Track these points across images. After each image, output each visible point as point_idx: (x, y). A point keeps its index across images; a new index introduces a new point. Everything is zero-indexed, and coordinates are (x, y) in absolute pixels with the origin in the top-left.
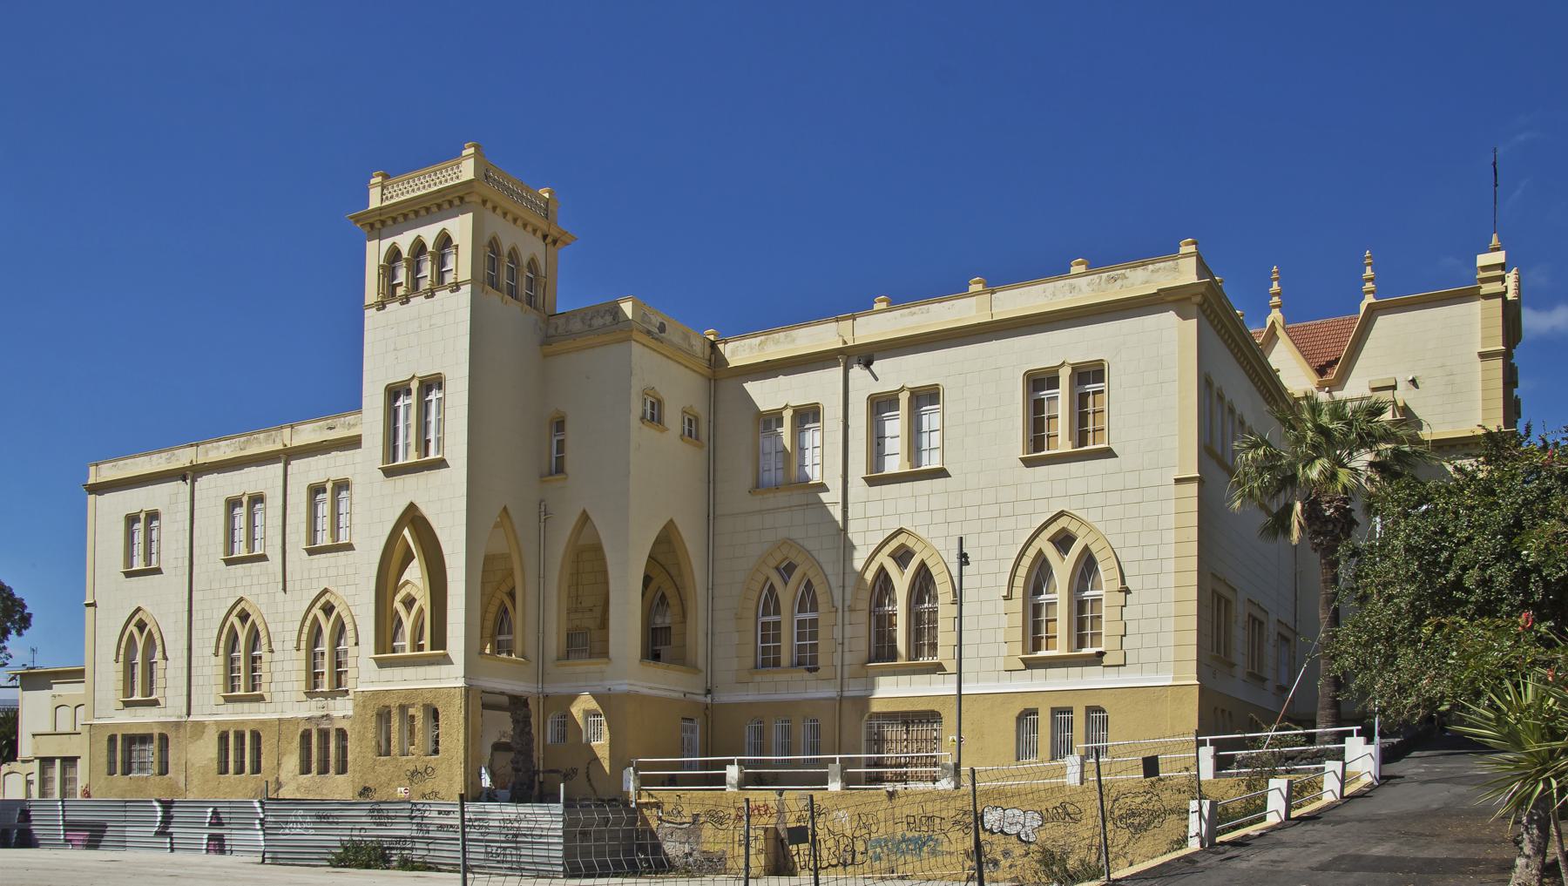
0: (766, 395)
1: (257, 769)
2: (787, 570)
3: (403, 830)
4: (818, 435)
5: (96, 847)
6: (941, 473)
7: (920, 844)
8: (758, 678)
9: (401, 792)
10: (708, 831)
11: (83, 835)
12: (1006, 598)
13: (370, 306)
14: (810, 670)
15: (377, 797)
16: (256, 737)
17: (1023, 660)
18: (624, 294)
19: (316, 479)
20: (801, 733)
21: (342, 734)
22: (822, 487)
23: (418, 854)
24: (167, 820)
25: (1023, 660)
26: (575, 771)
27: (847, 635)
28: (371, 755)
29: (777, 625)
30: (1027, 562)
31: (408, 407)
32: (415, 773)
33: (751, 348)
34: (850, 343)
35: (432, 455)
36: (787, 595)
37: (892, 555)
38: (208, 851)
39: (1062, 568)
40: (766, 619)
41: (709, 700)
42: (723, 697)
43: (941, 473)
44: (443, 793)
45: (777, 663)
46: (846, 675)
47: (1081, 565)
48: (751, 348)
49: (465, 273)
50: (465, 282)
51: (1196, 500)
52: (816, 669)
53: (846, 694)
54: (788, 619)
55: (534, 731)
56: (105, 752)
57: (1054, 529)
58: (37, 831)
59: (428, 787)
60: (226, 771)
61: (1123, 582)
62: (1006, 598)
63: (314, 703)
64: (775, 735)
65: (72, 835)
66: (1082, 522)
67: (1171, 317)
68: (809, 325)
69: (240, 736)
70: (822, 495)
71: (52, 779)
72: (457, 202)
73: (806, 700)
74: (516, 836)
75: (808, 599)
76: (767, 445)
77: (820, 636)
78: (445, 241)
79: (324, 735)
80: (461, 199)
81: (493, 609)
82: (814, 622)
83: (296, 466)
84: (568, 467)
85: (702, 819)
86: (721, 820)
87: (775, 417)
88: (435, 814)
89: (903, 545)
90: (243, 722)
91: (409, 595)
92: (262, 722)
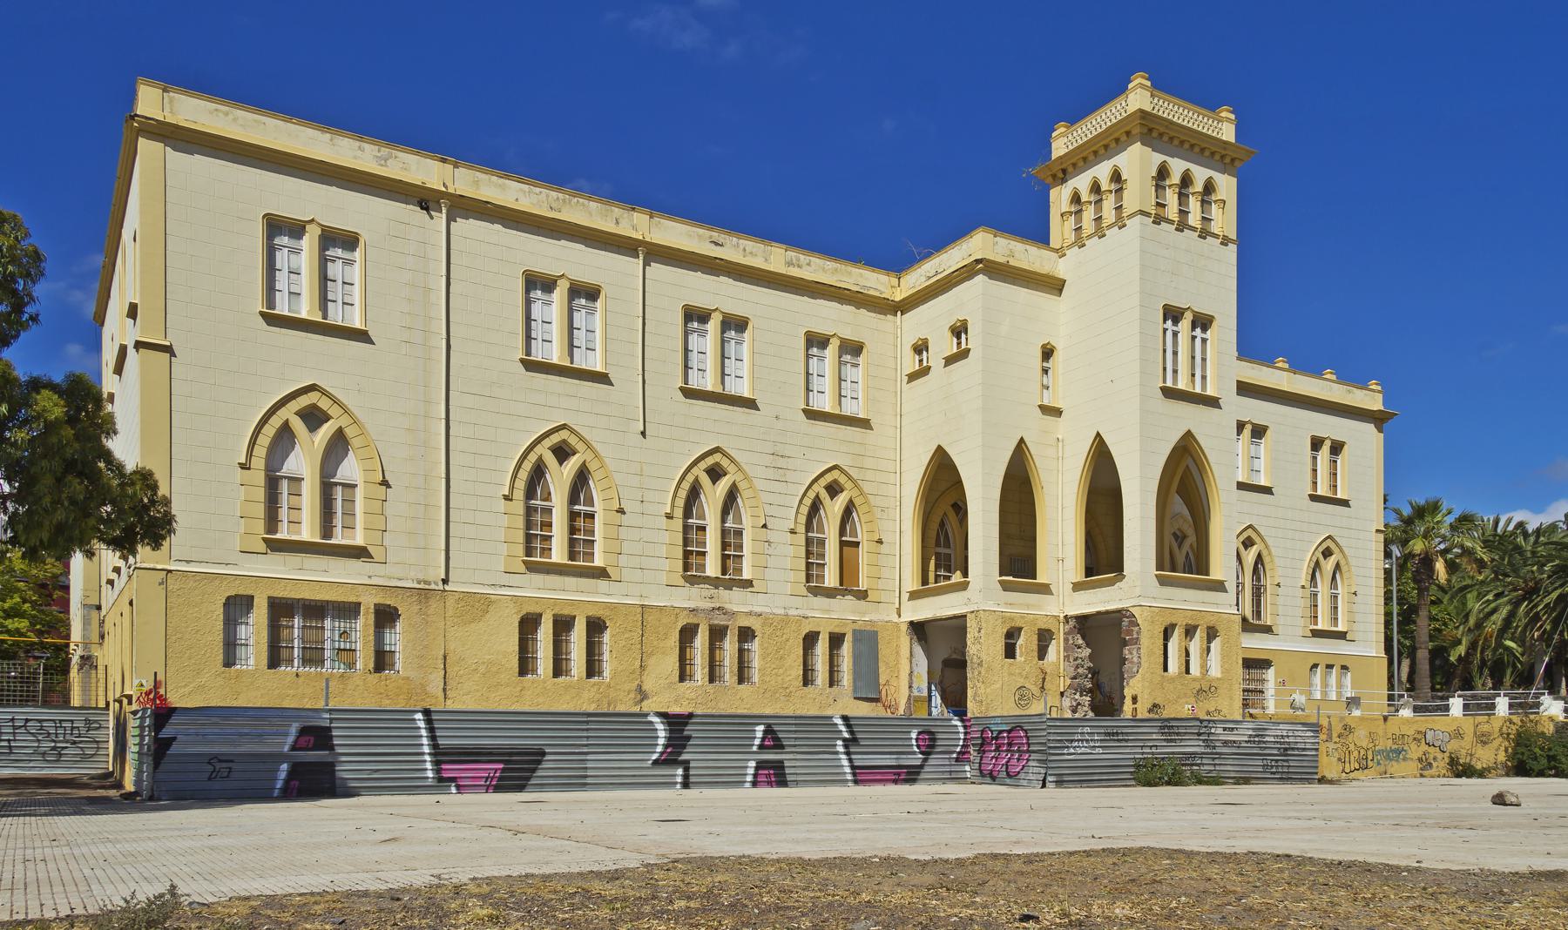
1: (593, 669)
3: (1193, 746)
5: (520, 788)
7: (1398, 752)
12: (244, 467)
15: (1165, 715)
17: (264, 540)
23: (1206, 769)
25: (264, 540)
38: (755, 784)
44: (1225, 711)
56: (220, 625)
58: (346, 770)
62: (244, 467)
63: (695, 590)
65: (450, 770)
67: (1370, 428)
88: (1220, 731)
91: (835, 481)
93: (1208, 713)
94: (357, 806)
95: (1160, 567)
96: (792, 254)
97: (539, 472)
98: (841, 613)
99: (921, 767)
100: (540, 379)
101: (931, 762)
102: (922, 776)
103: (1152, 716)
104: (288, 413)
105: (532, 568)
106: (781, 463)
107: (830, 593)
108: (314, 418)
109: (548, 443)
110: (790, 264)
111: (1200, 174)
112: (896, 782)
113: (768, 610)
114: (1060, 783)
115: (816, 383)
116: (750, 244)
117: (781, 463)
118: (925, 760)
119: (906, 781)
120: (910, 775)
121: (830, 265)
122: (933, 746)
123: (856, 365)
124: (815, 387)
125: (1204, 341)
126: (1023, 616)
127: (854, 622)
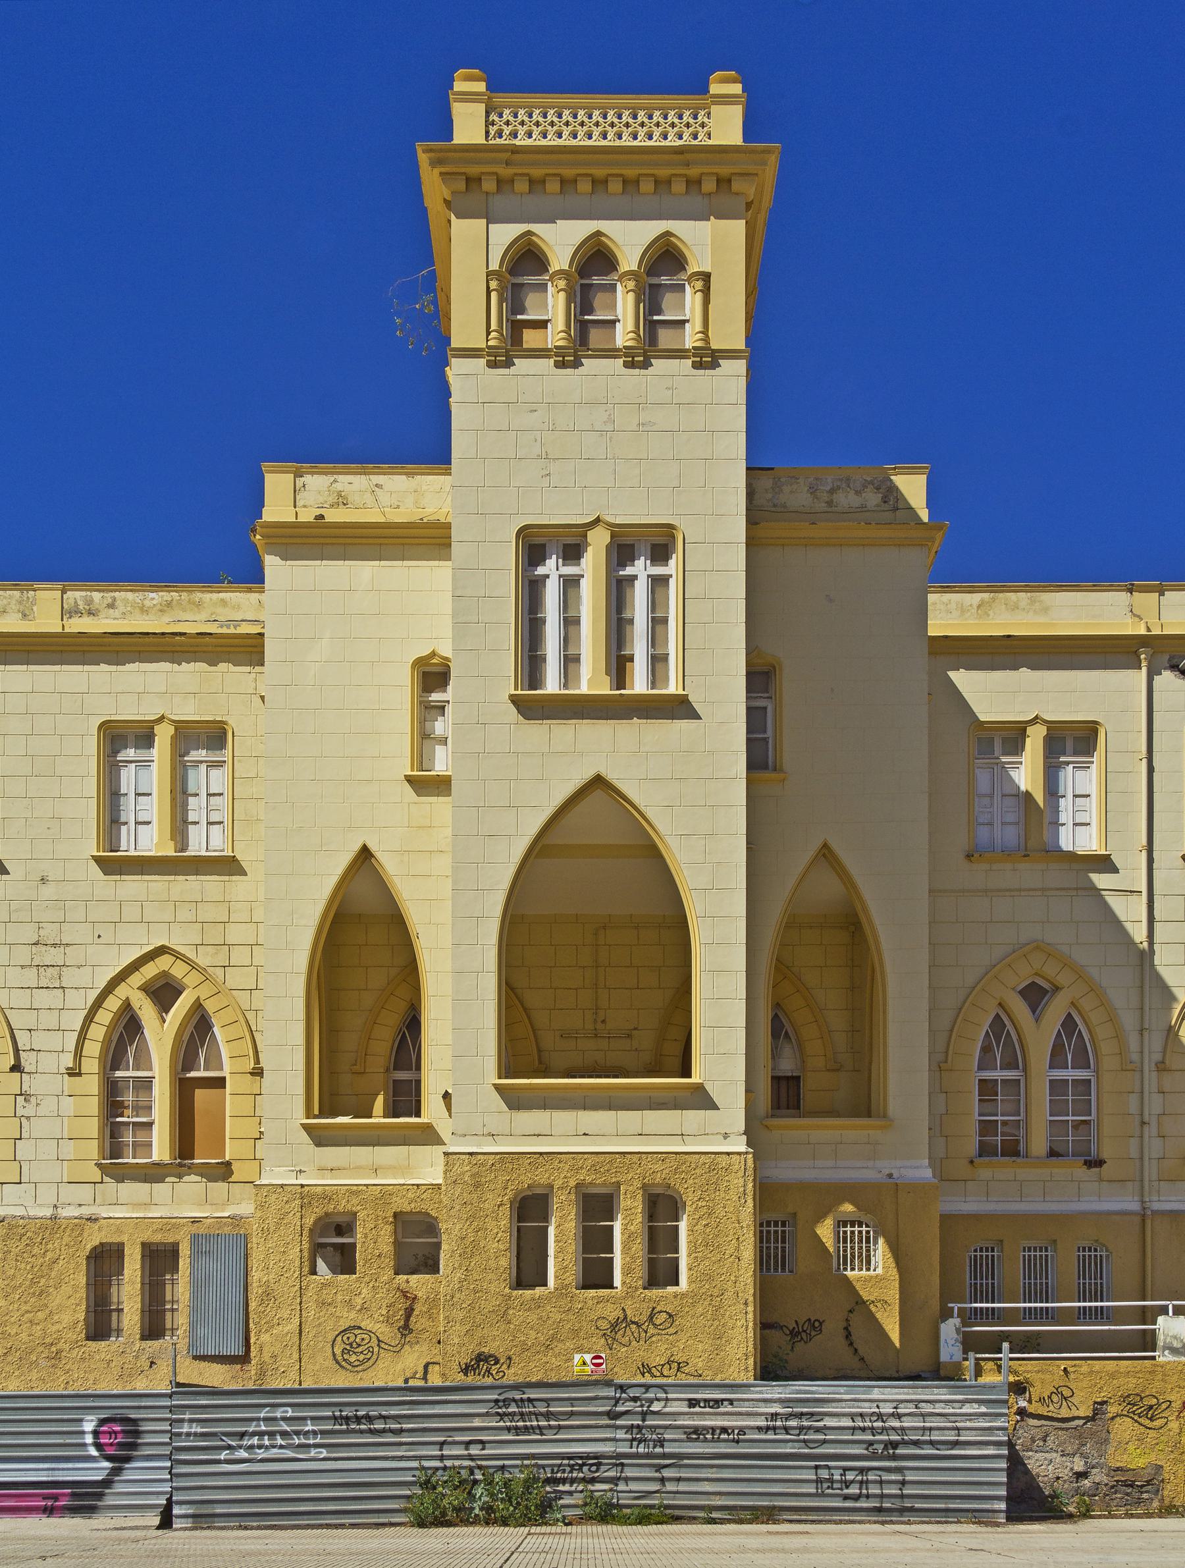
0: (989, 694)
2: (1035, 995)
4: (218, 780)
6: (229, 866)
8: (985, 1173)
9: (581, 1363)
10: (1123, 1429)
12: (74, 1072)
13: (732, 354)
15: (512, 1375)
18: (908, 459)
20: (1066, 1264)
22: (1105, 864)
23: (636, 1485)
26: (816, 1326)
30: (104, 1017)
31: (570, 584)
33: (963, 610)
34: (1156, 631)
35: (639, 684)
36: (1039, 1035)
37: (144, 988)
39: (160, 1035)
43: (229, 866)
47: (190, 1028)
48: (963, 610)
49: (731, 331)
50: (732, 354)
57: (150, 971)
61: (257, 1061)
64: (1013, 1269)
66: (193, 965)
68: (1060, 589)
70: (1101, 880)
72: (709, 186)
73: (1084, 1214)
74: (895, 1445)
75: (1071, 1044)
76: (983, 781)
78: (666, 259)
80: (724, 183)
85: (1112, 1410)
86: (1151, 1412)
87: (1013, 736)
89: (165, 974)
93: (645, 1369)
94: (747, 1534)
95: (506, 1069)
96: (75, 596)
97: (129, 1027)
98: (182, 1203)
99: (107, 1483)
100: (133, 885)
101: (127, 1475)
102: (109, 1501)
103: (471, 1379)
104: (131, 991)
105: (121, 1174)
106: (52, 956)
107: (153, 1174)
108: (164, 993)
109: (137, 979)
110: (67, 613)
111: (630, 240)
112: (49, 1511)
113: (19, 1212)
114: (202, 1519)
115: (129, 809)
116: (126, 597)
117: (52, 956)
118: (116, 1471)
119: (74, 1510)
120: (84, 1500)
121: (155, 598)
122: (134, 1446)
123: (219, 764)
124: (128, 815)
125: (659, 583)
126: (353, 1191)
127: (195, 1221)
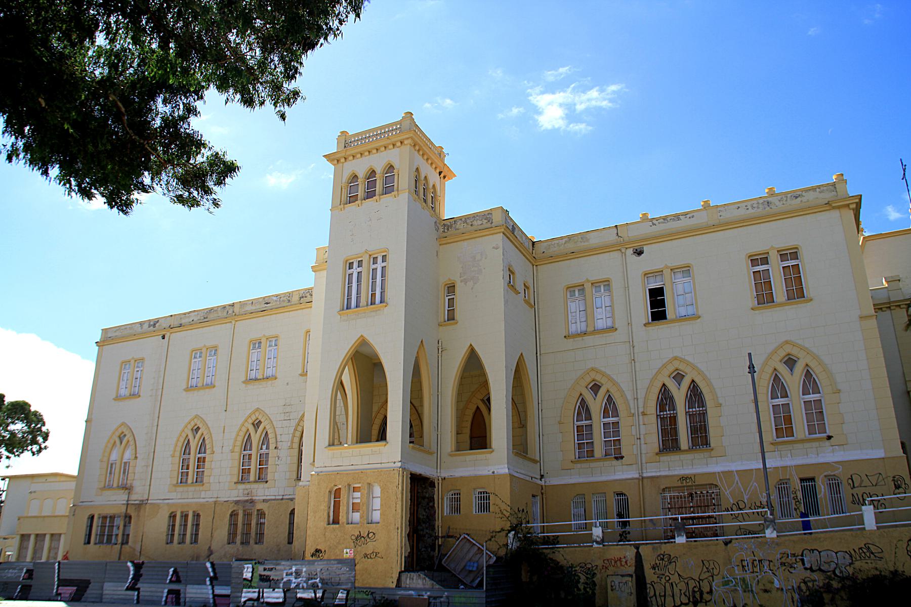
2: (596, 388)
11: (69, 590)
14: (616, 458)
16: (197, 516)
19: (758, 248)
21: (261, 514)
24: (137, 577)
27: (643, 432)
28: (323, 524)
29: (250, 455)
32: (359, 537)
40: (579, 423)
41: (543, 483)
42: (553, 481)
45: (591, 454)
46: (644, 461)
51: (877, 330)
52: (622, 457)
53: (645, 475)
54: (598, 421)
55: (436, 505)
59: (370, 547)
60: (89, 542)
65: (62, 590)
69: (185, 516)
71: (27, 548)
77: (270, 463)
79: (248, 515)
81: (470, 413)
82: (250, 455)
83: (242, 325)
84: (458, 315)
90: (188, 505)
92: (202, 505)
